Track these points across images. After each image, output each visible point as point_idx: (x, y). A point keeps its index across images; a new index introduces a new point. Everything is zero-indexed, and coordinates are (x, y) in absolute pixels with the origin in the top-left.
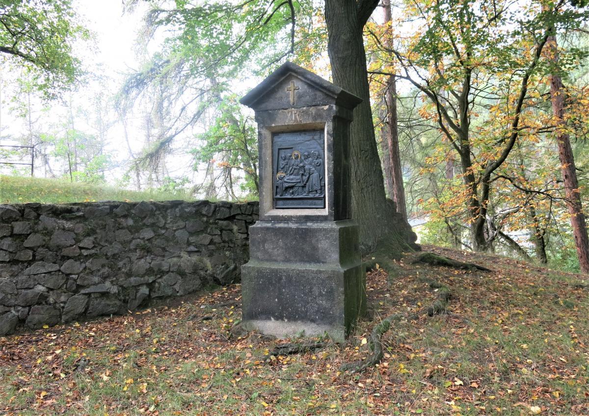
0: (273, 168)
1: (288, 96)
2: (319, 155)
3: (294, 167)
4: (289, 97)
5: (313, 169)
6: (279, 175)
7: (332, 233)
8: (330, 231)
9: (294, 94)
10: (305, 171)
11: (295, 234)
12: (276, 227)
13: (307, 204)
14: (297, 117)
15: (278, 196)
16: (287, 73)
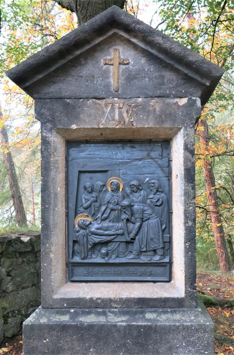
0: (67, 207)
1: (105, 74)
2: (160, 186)
3: (111, 206)
4: (108, 78)
5: (149, 211)
6: (80, 219)
7: (197, 335)
8: (197, 330)
9: (118, 72)
10: (132, 214)
11: (125, 337)
12: (82, 324)
13: (135, 275)
14: (125, 115)
15: (77, 259)
16: (107, 31)
